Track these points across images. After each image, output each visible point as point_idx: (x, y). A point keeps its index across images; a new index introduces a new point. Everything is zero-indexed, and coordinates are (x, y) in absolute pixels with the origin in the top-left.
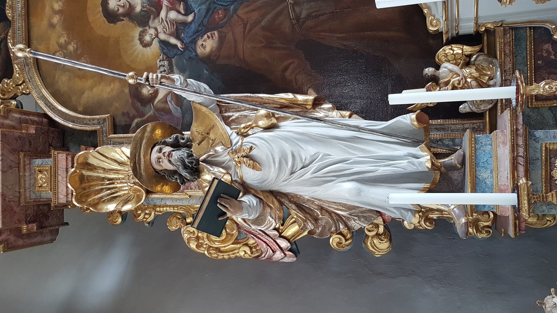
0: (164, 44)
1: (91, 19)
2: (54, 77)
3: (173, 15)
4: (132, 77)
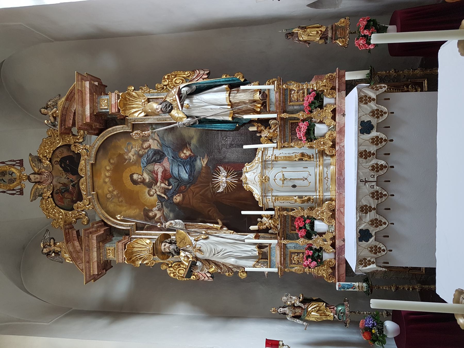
0: (159, 196)
1: (125, 182)
2: (107, 205)
3: (163, 185)
4: (159, 225)
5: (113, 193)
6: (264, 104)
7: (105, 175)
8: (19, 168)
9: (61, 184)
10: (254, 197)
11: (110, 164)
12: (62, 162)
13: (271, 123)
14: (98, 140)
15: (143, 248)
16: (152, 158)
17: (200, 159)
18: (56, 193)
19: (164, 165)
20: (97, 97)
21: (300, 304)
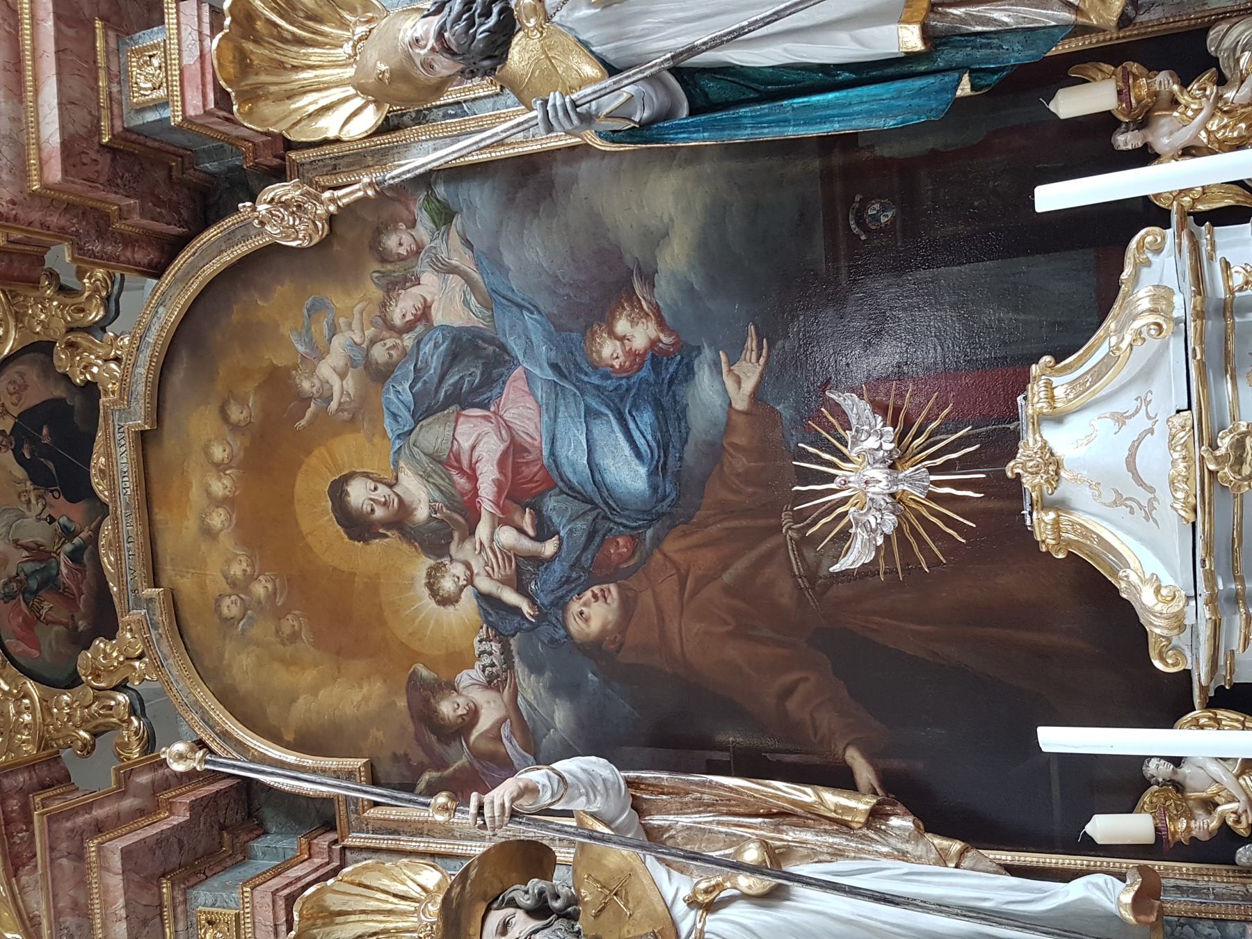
0: (488, 601)
2: (221, 656)
3: (507, 536)
5: (247, 590)
7: (208, 493)
9: (26, 548)
11: (226, 429)
13: (1227, 43)
14: (159, 304)
15: (403, 913)
16: (442, 379)
17: (716, 364)
19: (507, 416)
20: (113, 44)
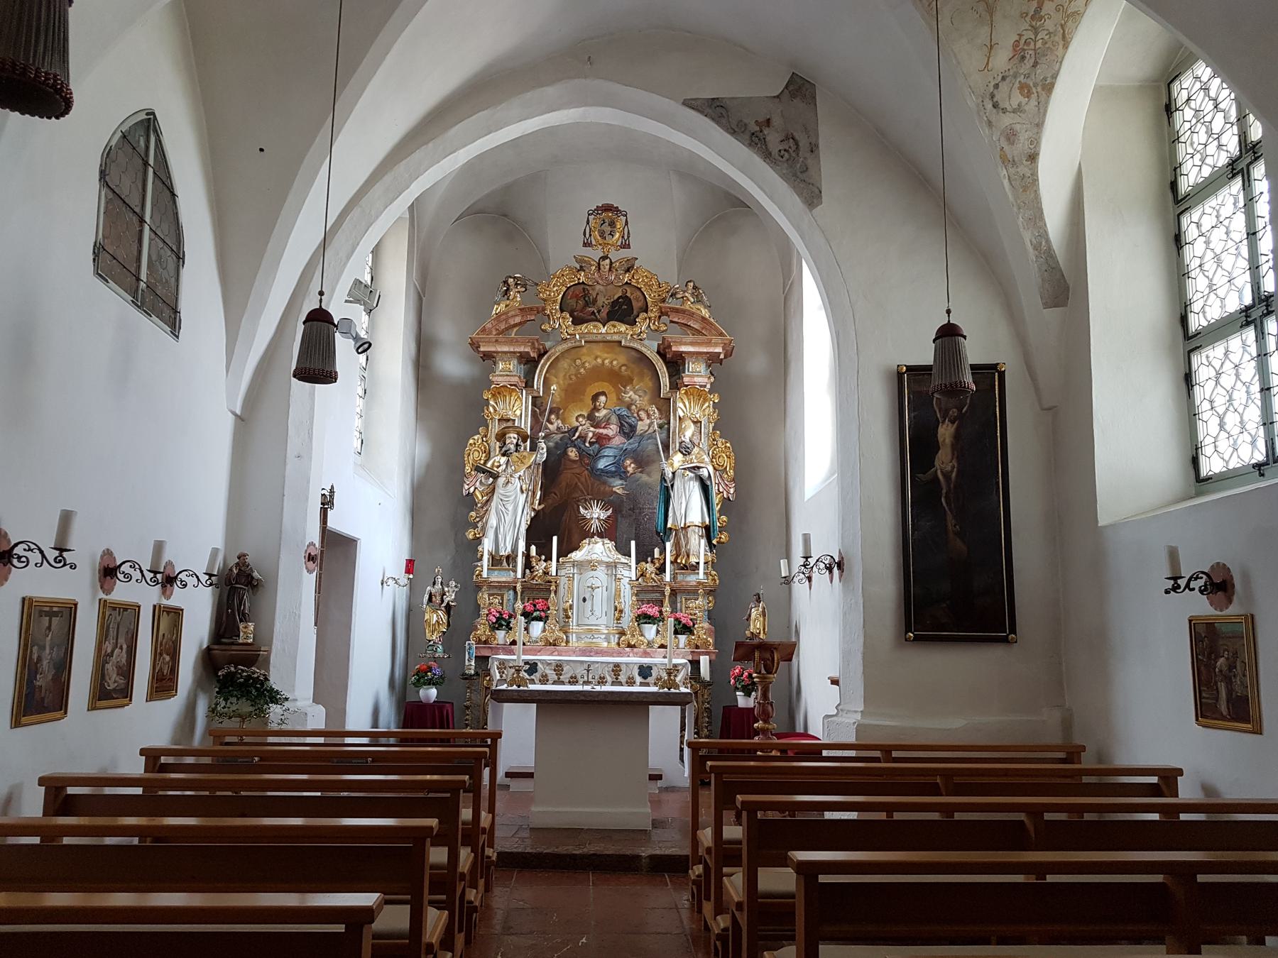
0: (577, 428)
1: (596, 384)
2: (567, 358)
3: (590, 435)
6: (685, 567)
8: (619, 243)
10: (572, 552)
12: (626, 299)
18: (584, 289)
21: (446, 602)
